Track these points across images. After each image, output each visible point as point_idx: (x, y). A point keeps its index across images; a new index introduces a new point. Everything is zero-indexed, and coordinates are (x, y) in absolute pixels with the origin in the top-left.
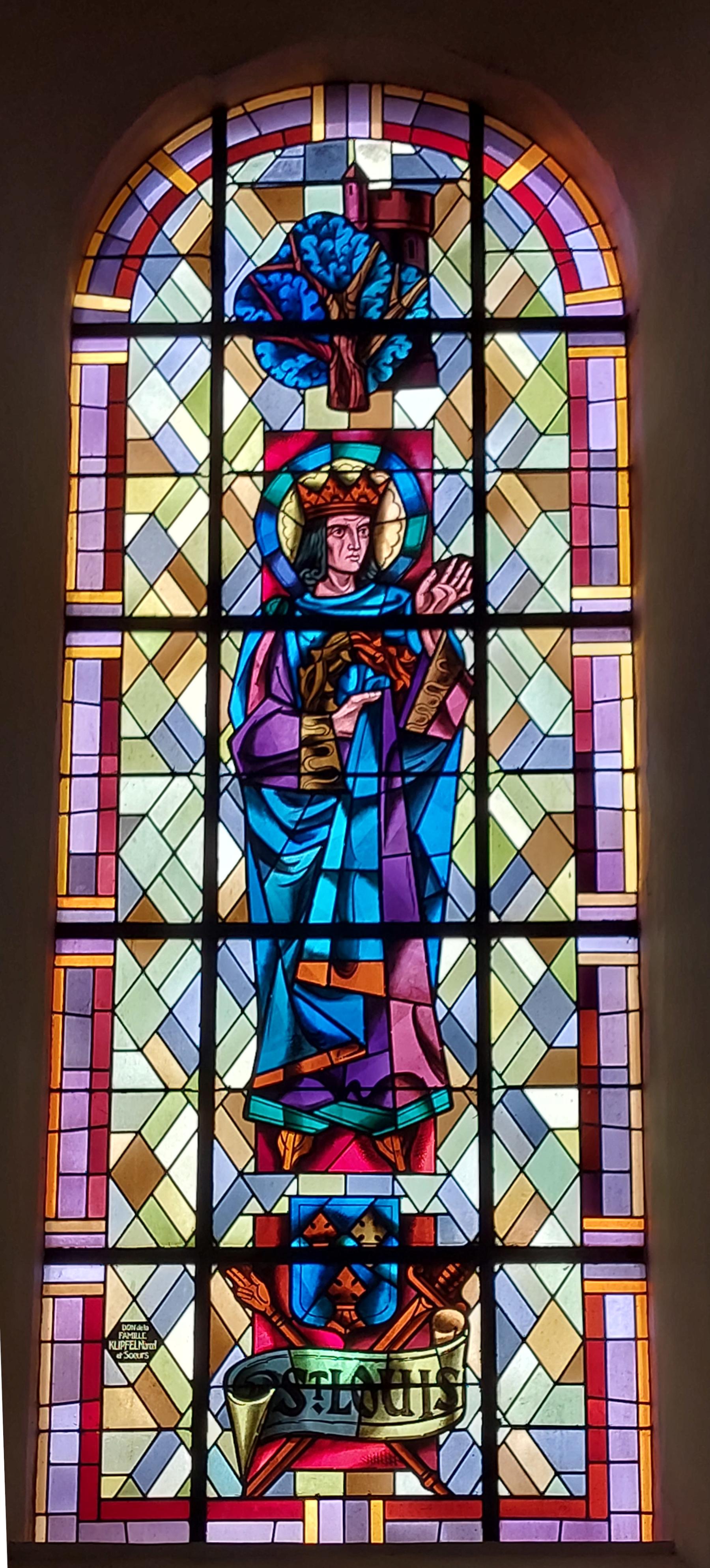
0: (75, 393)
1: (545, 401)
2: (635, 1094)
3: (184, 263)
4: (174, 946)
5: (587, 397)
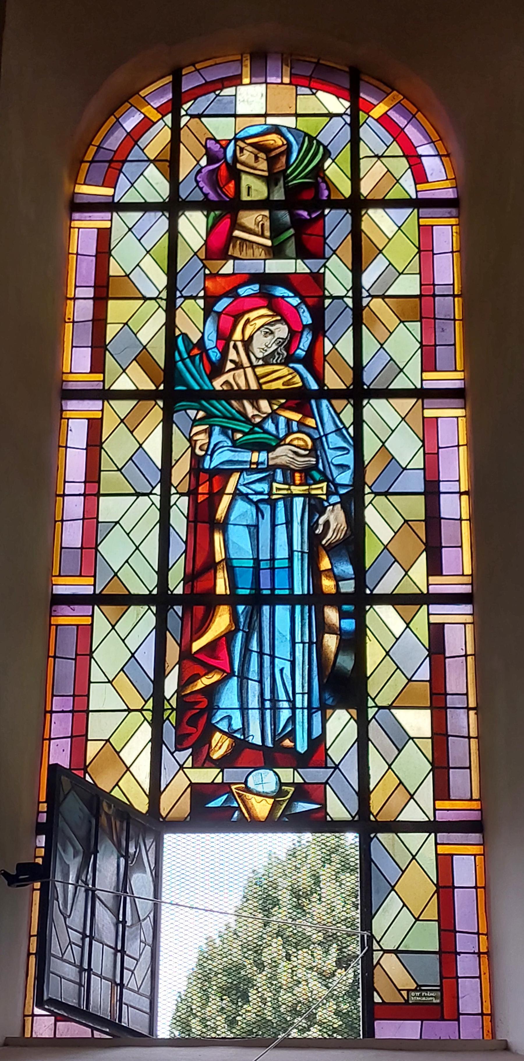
0: (72, 270)
1: (403, 252)
2: (465, 498)
3: (152, 165)
4: (134, 611)
5: (433, 250)
